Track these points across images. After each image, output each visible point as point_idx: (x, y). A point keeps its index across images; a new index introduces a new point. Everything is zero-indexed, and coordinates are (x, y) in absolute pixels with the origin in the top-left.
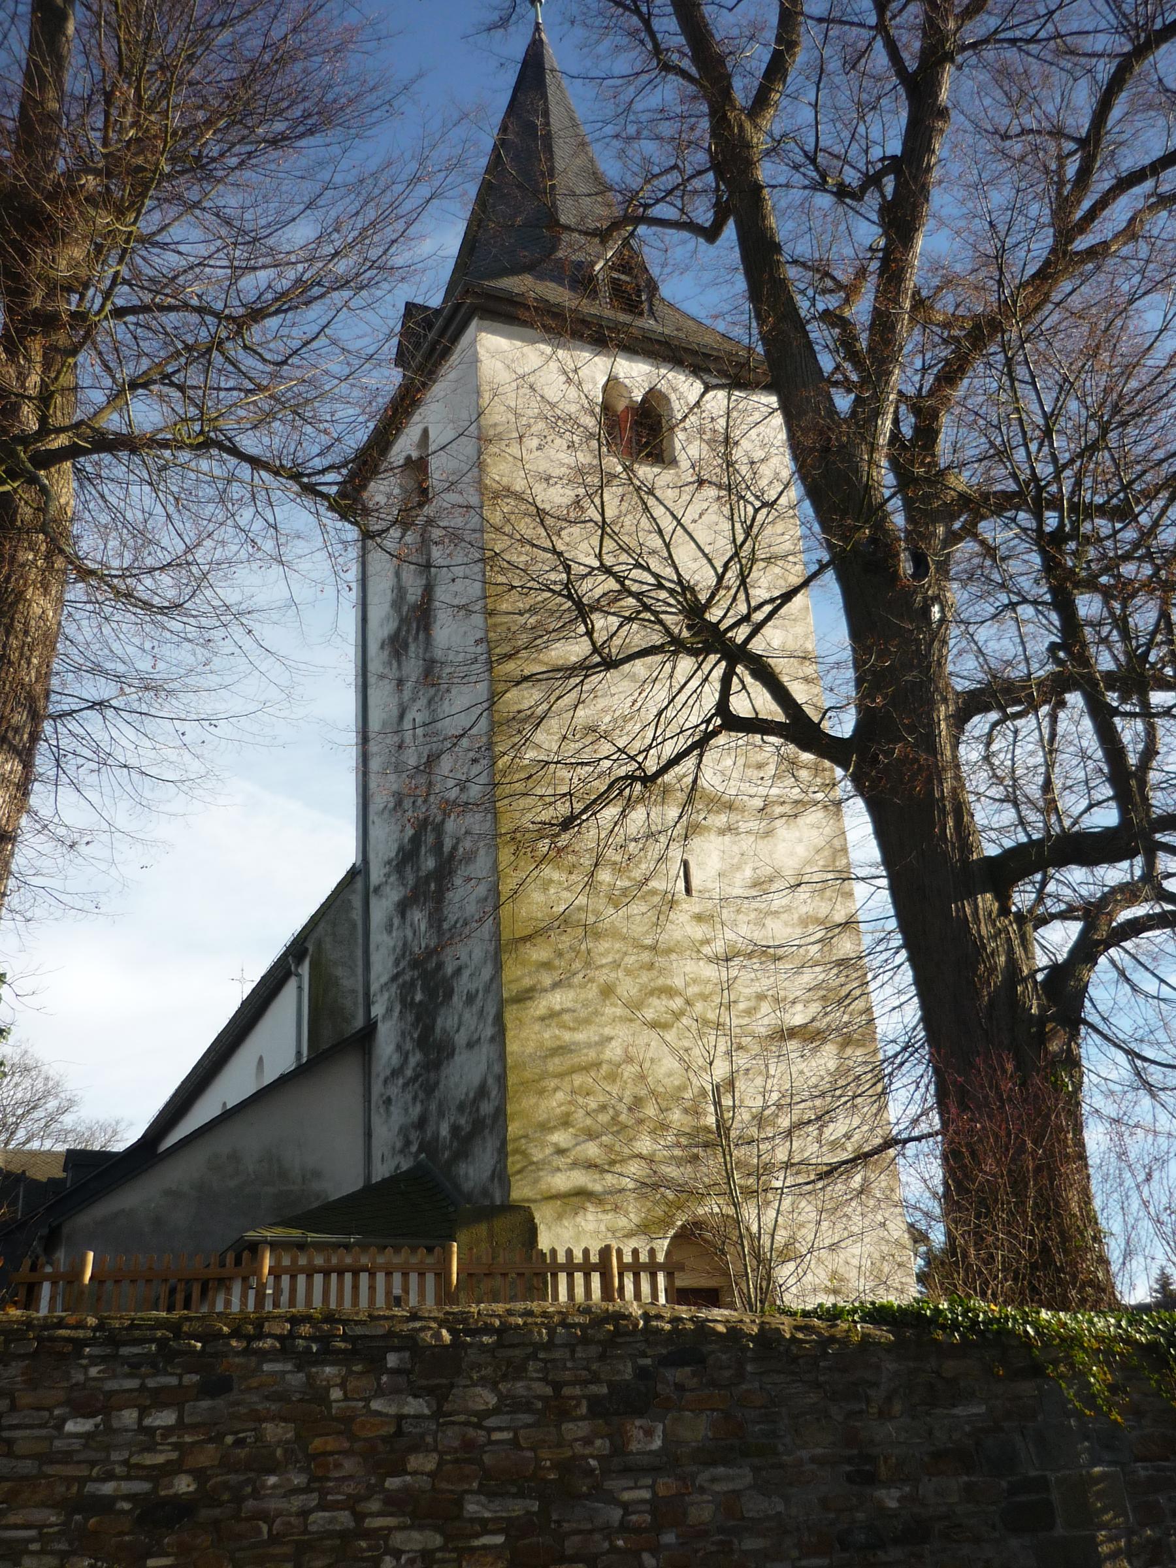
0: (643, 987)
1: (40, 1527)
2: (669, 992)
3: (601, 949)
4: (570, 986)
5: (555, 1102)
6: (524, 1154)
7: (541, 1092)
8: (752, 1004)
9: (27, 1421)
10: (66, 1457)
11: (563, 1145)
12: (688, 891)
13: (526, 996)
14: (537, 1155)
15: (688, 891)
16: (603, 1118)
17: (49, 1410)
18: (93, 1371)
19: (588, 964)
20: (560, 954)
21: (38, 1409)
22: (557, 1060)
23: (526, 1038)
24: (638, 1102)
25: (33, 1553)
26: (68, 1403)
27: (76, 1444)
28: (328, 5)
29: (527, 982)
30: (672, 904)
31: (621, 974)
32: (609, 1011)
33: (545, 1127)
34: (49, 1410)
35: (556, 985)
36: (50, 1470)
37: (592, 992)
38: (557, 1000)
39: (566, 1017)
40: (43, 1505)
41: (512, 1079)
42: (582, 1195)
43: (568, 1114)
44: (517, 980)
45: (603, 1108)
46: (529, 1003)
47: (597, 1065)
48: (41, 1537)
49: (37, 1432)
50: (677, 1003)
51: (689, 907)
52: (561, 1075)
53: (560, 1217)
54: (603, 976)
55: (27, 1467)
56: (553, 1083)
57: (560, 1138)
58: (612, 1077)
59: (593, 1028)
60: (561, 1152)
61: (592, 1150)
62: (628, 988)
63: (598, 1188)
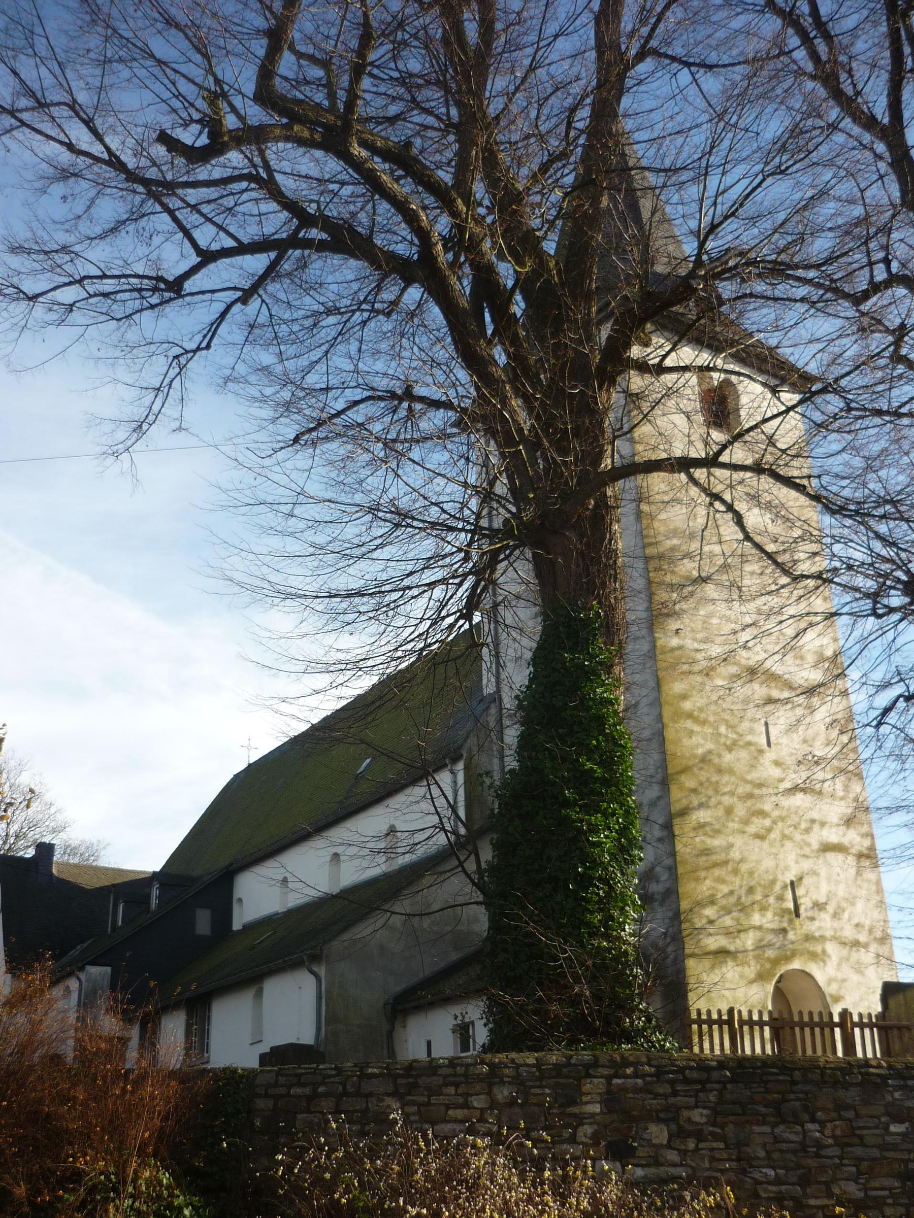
0: (748, 810)
1: (890, 1189)
2: (762, 814)
3: (724, 782)
4: (708, 807)
5: (705, 888)
6: (689, 921)
7: (697, 879)
8: (808, 825)
9: (868, 1125)
10: (895, 1147)
11: (712, 918)
12: (769, 744)
13: (684, 812)
14: (699, 923)
15: (769, 744)
16: (732, 900)
17: (878, 1117)
18: (897, 1095)
19: (717, 791)
20: (701, 784)
21: (872, 1117)
22: (704, 858)
23: (687, 844)
24: (751, 890)
25: (889, 1205)
26: (887, 1114)
27: (898, 1139)
28: (798, 4)
29: (684, 802)
30: (761, 752)
31: (735, 799)
32: (731, 825)
33: (700, 904)
34: (878, 1117)
35: (701, 805)
36: (889, 1154)
37: (720, 812)
38: (702, 816)
39: (708, 829)
40: (888, 1176)
41: (680, 870)
42: (723, 953)
43: (713, 895)
44: (678, 801)
45: (732, 893)
46: (686, 817)
47: (726, 862)
48: (892, 1195)
49: (874, 1131)
50: (767, 822)
51: (770, 755)
52: (707, 869)
53: (713, 967)
54: (727, 800)
55: (875, 1153)
56: (703, 874)
57: (710, 912)
58: (736, 872)
59: (723, 836)
60: (711, 922)
61: (728, 921)
62: (740, 810)
63: (732, 948)
